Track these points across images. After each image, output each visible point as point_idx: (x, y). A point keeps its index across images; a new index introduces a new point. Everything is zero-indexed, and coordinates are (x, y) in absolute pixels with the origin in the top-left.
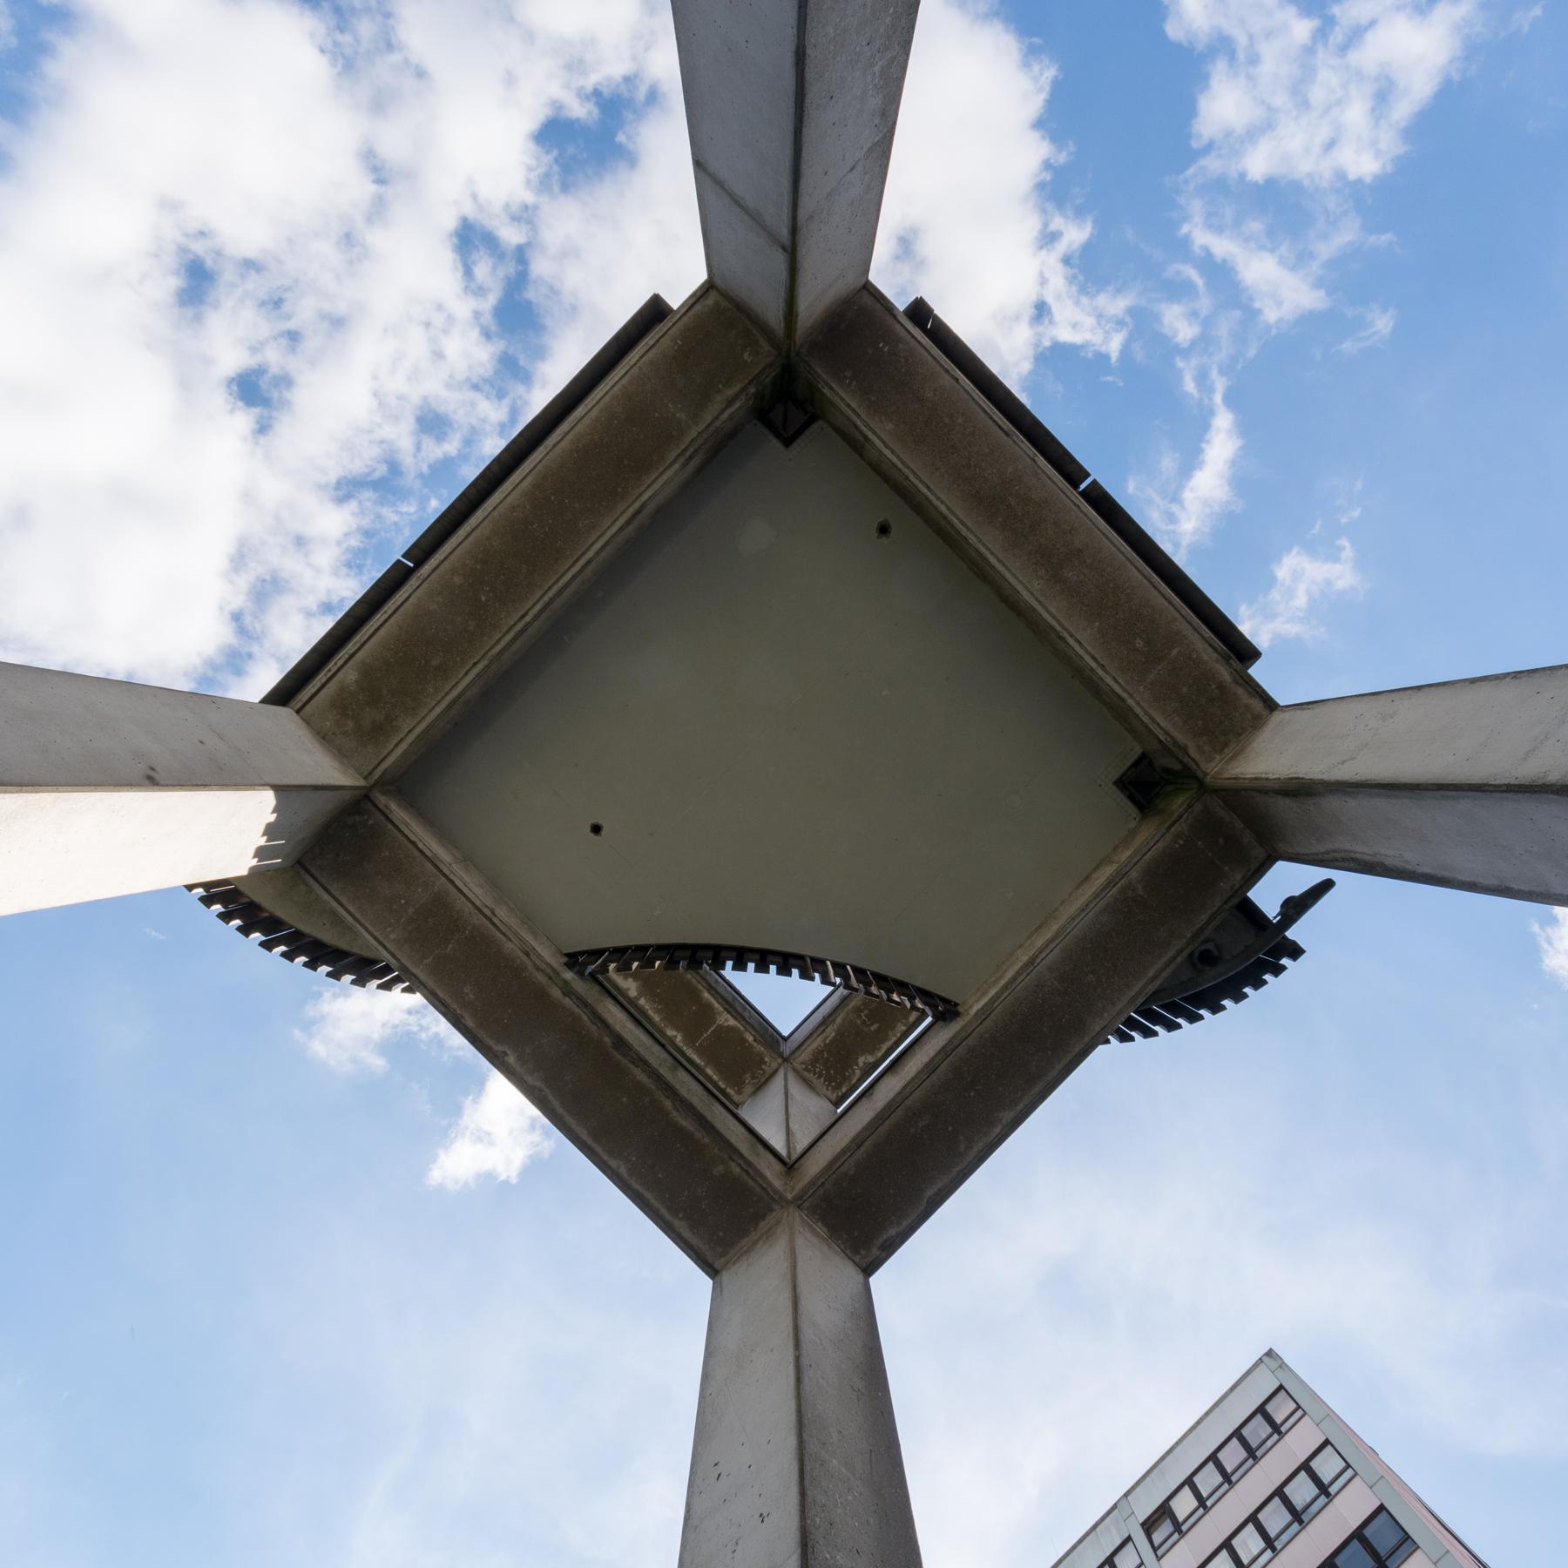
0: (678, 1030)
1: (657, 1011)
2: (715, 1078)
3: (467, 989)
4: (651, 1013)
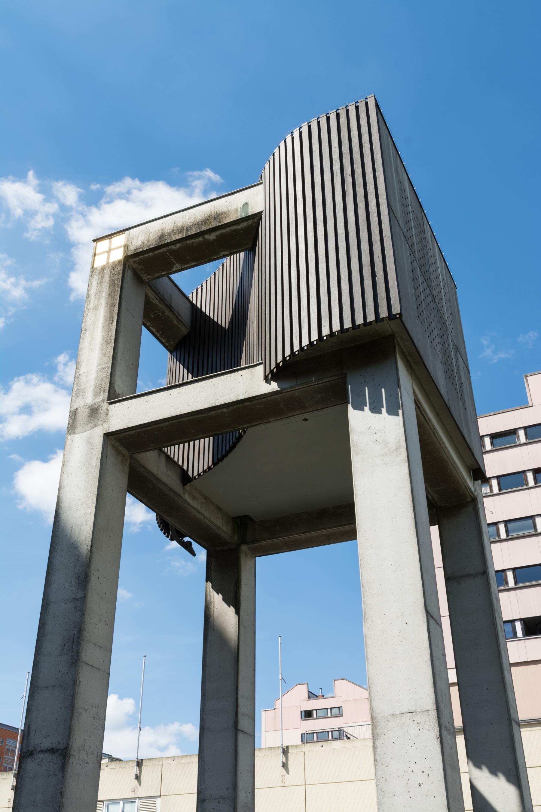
0: (178, 249)
1: (193, 243)
2: (146, 255)
3: (261, 406)
4: (193, 240)
